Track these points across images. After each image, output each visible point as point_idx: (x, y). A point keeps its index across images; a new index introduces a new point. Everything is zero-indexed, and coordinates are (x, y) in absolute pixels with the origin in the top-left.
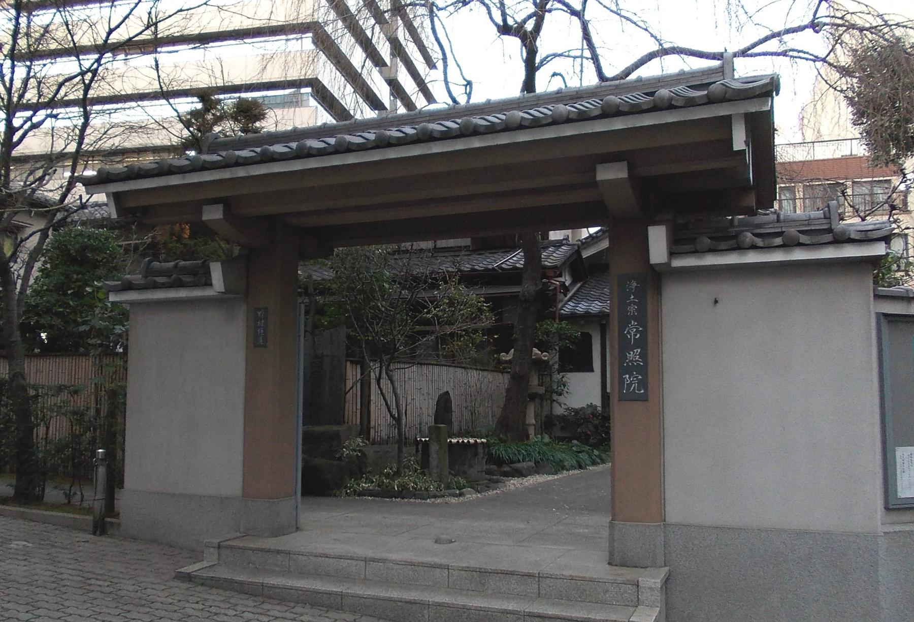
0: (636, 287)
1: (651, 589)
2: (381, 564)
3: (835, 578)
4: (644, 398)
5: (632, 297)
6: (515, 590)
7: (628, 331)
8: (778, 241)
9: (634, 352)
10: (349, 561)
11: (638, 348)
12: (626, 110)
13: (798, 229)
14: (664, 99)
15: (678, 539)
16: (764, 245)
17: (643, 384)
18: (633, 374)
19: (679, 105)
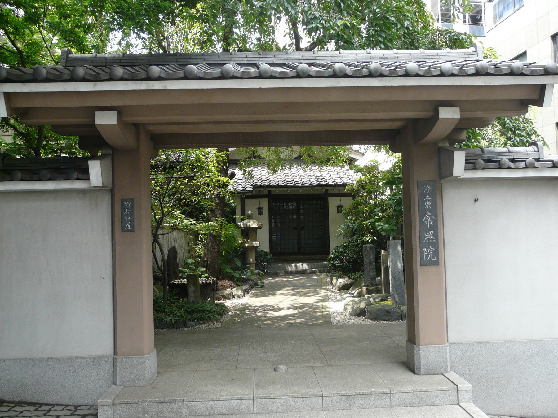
0: (430, 190)
1: (467, 391)
2: (267, 400)
3: (313, 358)
4: (437, 263)
5: (428, 197)
6: (374, 405)
7: (426, 219)
8: (522, 165)
9: (429, 233)
10: (239, 401)
12: (351, 74)
13: (509, 158)
14: (519, 68)
16: (515, 167)
17: (436, 253)
18: (429, 248)
19: (527, 74)
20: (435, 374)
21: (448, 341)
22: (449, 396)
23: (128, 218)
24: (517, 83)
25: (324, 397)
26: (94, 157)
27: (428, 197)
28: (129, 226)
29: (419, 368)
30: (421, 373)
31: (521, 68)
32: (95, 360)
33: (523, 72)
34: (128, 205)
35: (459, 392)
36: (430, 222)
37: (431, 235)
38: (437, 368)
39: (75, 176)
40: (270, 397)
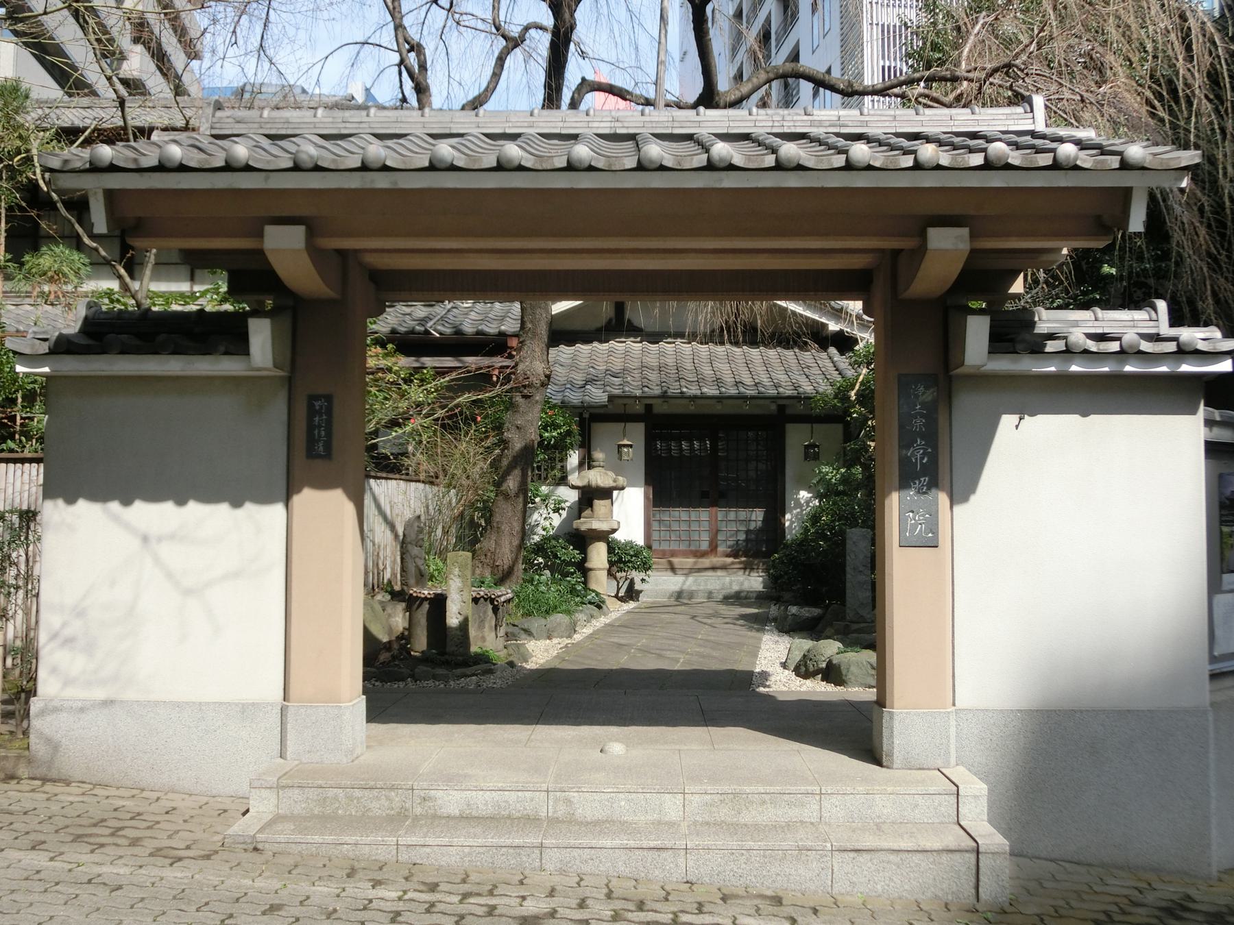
1: (975, 797)
5: (918, 407)
10: (520, 794)
11: (925, 476)
14: (1070, 155)
15: (972, 728)
16: (1099, 349)
19: (1086, 167)
20: (923, 769)
21: (954, 705)
22: (940, 805)
23: (319, 433)
24: (1070, 185)
25: (686, 795)
26: (257, 313)
27: (918, 407)
28: (320, 447)
29: (891, 755)
30: (895, 766)
31: (1072, 156)
32: (247, 710)
33: (1079, 163)
34: (321, 407)
35: (960, 797)
36: (922, 459)
37: (923, 485)
38: (927, 756)
39: (222, 349)
40: (580, 788)
